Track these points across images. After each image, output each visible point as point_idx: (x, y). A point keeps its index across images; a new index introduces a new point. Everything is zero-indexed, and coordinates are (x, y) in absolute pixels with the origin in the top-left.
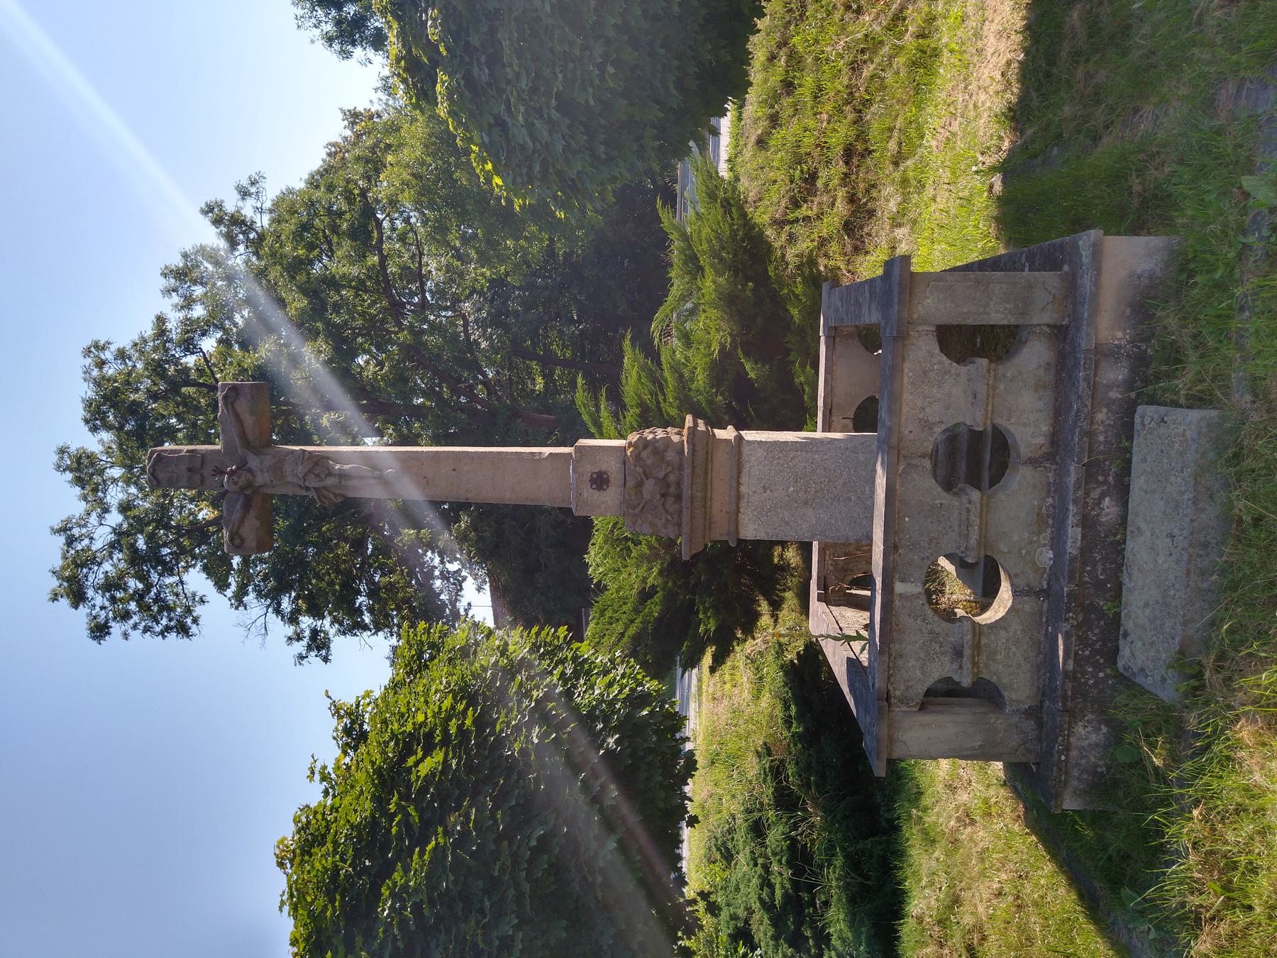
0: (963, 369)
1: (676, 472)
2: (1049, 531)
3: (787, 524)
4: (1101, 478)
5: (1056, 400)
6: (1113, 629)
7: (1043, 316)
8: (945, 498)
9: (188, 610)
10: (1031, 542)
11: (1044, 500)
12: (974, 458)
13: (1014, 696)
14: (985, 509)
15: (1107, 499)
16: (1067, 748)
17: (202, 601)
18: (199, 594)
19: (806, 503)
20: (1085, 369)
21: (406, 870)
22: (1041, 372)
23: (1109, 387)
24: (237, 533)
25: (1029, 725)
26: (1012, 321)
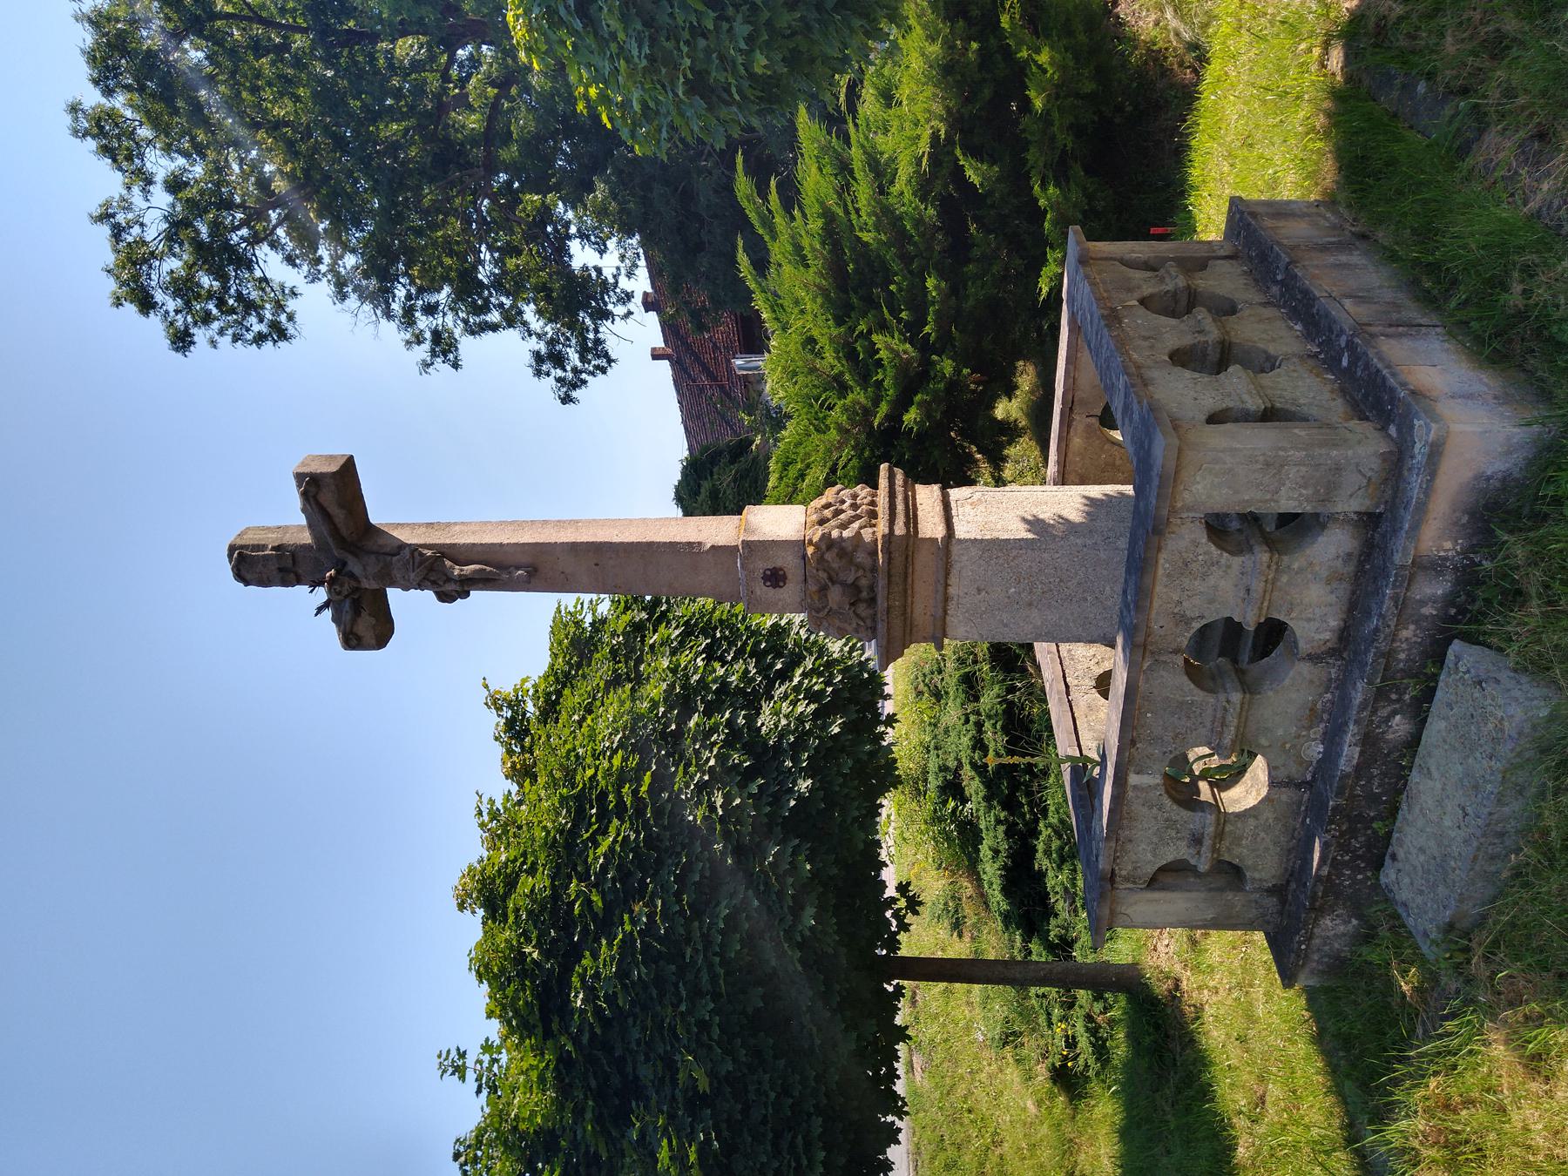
0: (1237, 561)
1: (869, 575)
2: (1322, 725)
3: (1006, 625)
4: (1394, 697)
5: (1353, 593)
6: (1378, 853)
7: (1350, 502)
8: (1199, 695)
9: (279, 307)
10: (1298, 736)
11: (1321, 695)
12: (1239, 650)
13: (1257, 875)
14: (1245, 709)
15: (1398, 717)
16: (1310, 938)
17: (294, 294)
18: (288, 285)
19: (1030, 604)
20: (1394, 586)
21: (595, 956)
22: (1339, 563)
23: (1423, 603)
24: (351, 632)
25: (1271, 902)
26: (1309, 509)
